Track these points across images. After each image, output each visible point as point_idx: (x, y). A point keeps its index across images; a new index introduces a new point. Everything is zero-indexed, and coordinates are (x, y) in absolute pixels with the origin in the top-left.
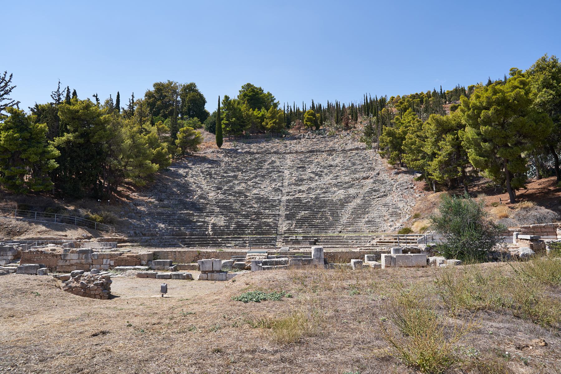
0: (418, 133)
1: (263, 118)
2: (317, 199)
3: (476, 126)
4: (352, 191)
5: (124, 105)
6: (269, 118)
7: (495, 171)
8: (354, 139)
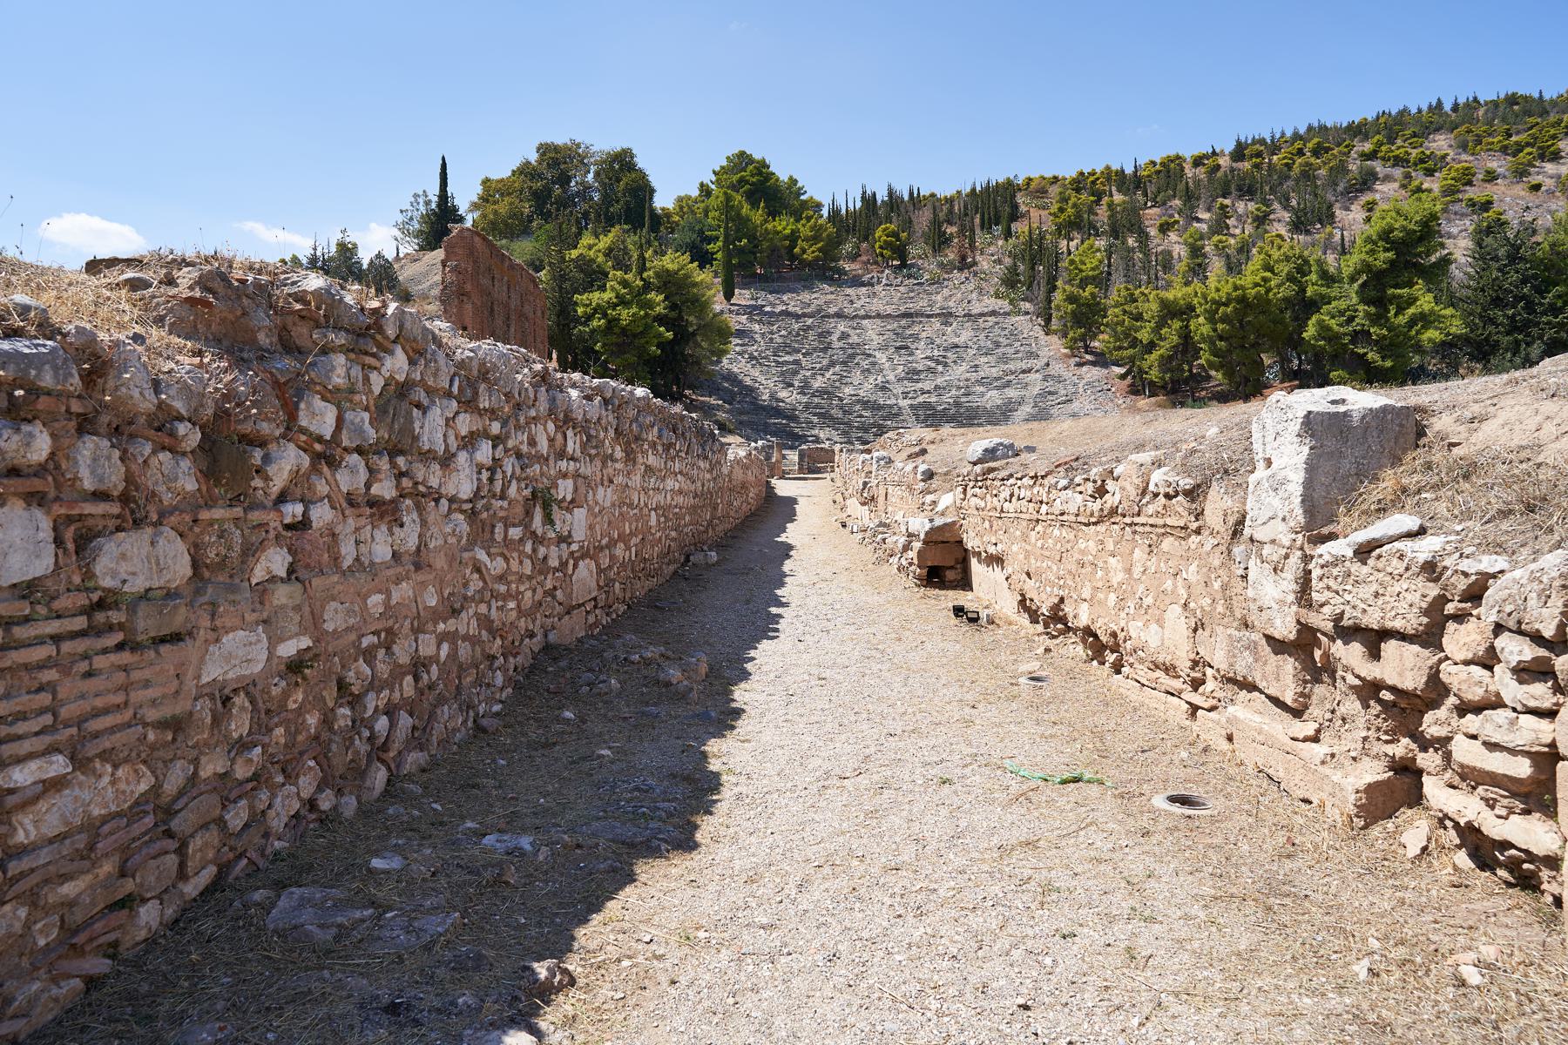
0: (1127, 308)
1: (794, 237)
2: (957, 404)
3: (1211, 319)
4: (1011, 393)
6: (806, 239)
7: (1230, 374)
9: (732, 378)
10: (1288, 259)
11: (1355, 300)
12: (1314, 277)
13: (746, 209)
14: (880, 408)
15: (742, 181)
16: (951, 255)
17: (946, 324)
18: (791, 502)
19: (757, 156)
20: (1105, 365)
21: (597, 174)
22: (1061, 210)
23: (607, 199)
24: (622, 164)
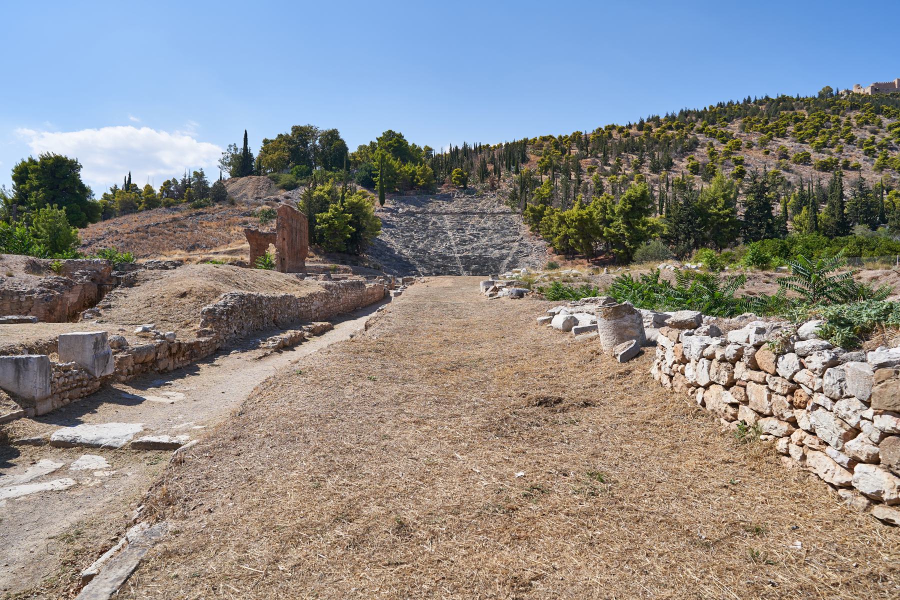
1: (414, 174)
2: (480, 256)
4: (504, 251)
5: (256, 150)
6: (420, 175)
8: (500, 202)
11: (620, 221)
13: (392, 161)
15: (390, 145)
19: (397, 132)
21: (320, 142)
22: (543, 160)
24: (332, 136)
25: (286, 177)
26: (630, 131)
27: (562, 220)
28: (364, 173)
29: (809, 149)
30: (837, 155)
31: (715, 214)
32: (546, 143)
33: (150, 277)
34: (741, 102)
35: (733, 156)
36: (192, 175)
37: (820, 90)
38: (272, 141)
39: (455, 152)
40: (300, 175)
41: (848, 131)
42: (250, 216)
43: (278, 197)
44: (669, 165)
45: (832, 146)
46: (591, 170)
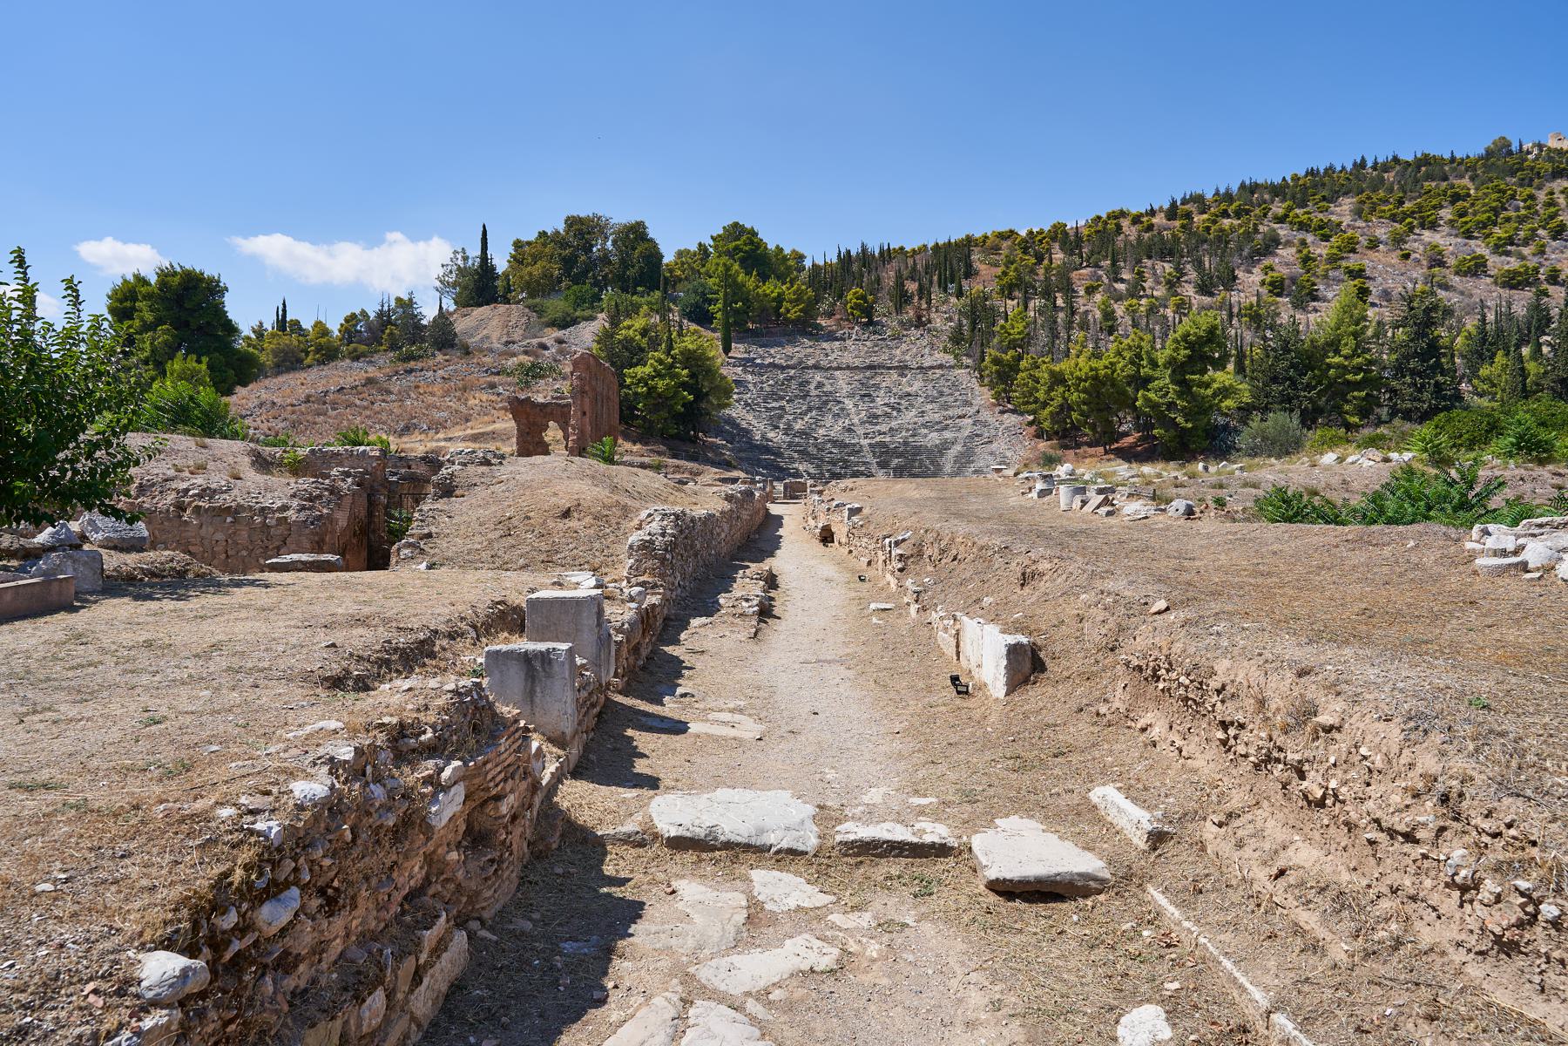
1: (780, 299)
2: (906, 443)
4: (948, 435)
6: (791, 301)
9: (731, 421)
10: (1130, 348)
11: (1167, 380)
12: (1144, 363)
14: (846, 446)
16: (910, 313)
17: (903, 375)
18: (781, 517)
19: (748, 226)
20: (1022, 414)
21: (614, 242)
22: (1005, 274)
23: (625, 264)
24: (636, 234)
25: (557, 305)
26: (1154, 220)
27: (1058, 379)
28: (693, 299)
29: (1480, 248)
30: (1536, 259)
31: (1338, 366)
32: (1005, 244)
33: (476, 480)
34: (1349, 167)
35: (1344, 263)
36: (393, 304)
37: (1488, 143)
38: (529, 243)
39: (846, 260)
40: (579, 302)
41: (1552, 217)
42: (498, 374)
43: (544, 340)
44: (1230, 281)
45: (1526, 242)
46: (1090, 291)
